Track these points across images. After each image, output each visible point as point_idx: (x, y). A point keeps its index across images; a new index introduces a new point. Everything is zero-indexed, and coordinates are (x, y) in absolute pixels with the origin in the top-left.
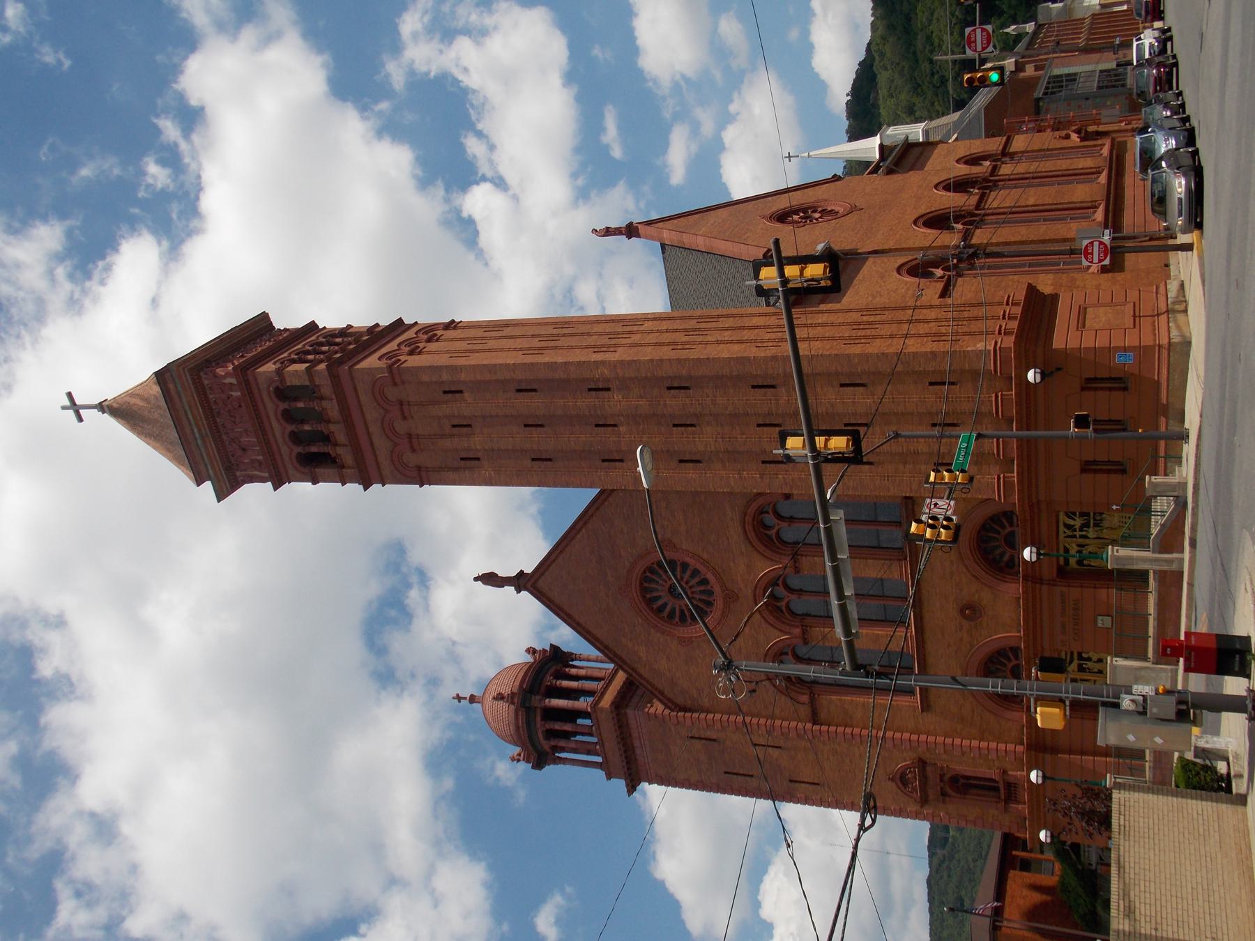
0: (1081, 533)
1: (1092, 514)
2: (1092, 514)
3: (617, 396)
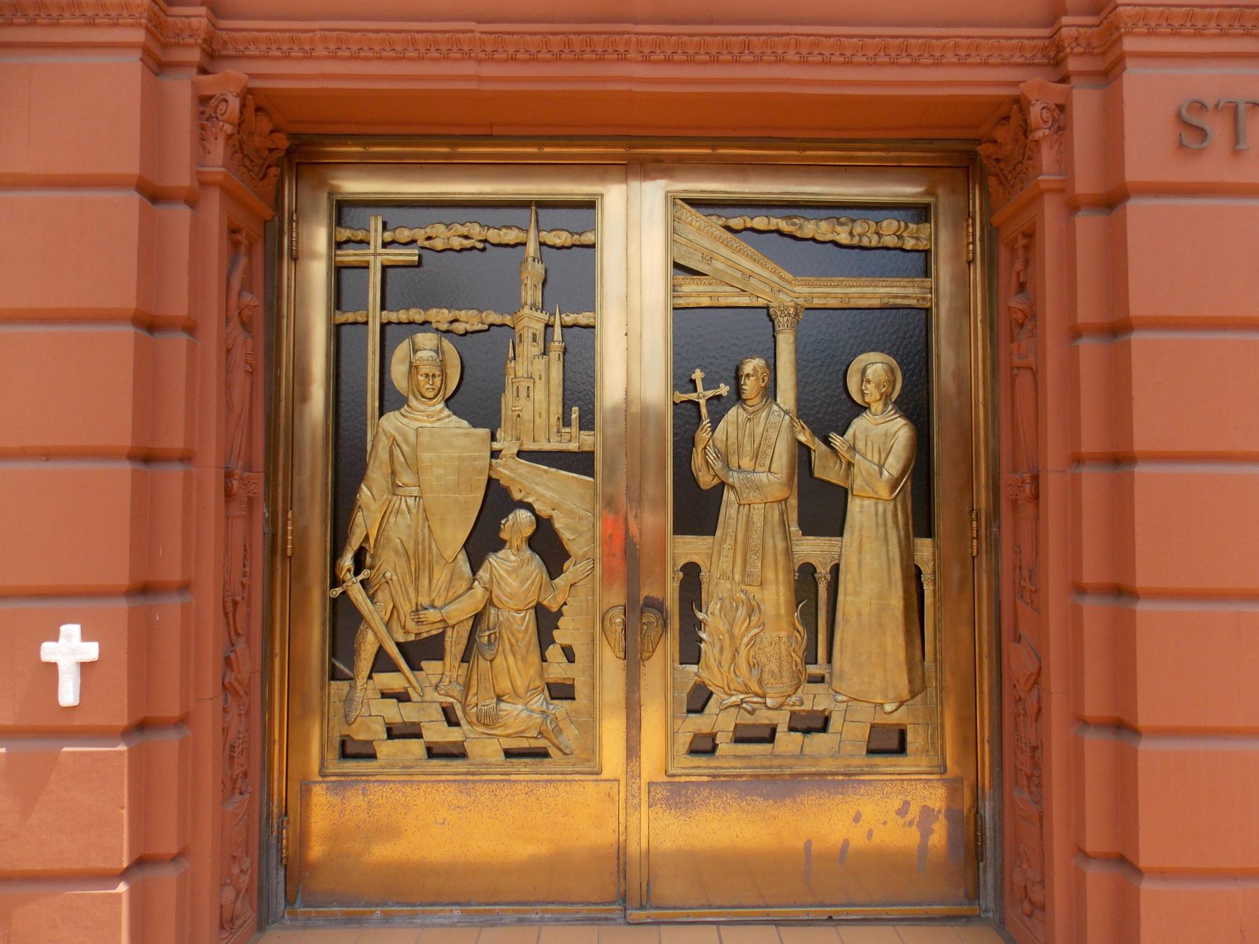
3: (1026, 795)
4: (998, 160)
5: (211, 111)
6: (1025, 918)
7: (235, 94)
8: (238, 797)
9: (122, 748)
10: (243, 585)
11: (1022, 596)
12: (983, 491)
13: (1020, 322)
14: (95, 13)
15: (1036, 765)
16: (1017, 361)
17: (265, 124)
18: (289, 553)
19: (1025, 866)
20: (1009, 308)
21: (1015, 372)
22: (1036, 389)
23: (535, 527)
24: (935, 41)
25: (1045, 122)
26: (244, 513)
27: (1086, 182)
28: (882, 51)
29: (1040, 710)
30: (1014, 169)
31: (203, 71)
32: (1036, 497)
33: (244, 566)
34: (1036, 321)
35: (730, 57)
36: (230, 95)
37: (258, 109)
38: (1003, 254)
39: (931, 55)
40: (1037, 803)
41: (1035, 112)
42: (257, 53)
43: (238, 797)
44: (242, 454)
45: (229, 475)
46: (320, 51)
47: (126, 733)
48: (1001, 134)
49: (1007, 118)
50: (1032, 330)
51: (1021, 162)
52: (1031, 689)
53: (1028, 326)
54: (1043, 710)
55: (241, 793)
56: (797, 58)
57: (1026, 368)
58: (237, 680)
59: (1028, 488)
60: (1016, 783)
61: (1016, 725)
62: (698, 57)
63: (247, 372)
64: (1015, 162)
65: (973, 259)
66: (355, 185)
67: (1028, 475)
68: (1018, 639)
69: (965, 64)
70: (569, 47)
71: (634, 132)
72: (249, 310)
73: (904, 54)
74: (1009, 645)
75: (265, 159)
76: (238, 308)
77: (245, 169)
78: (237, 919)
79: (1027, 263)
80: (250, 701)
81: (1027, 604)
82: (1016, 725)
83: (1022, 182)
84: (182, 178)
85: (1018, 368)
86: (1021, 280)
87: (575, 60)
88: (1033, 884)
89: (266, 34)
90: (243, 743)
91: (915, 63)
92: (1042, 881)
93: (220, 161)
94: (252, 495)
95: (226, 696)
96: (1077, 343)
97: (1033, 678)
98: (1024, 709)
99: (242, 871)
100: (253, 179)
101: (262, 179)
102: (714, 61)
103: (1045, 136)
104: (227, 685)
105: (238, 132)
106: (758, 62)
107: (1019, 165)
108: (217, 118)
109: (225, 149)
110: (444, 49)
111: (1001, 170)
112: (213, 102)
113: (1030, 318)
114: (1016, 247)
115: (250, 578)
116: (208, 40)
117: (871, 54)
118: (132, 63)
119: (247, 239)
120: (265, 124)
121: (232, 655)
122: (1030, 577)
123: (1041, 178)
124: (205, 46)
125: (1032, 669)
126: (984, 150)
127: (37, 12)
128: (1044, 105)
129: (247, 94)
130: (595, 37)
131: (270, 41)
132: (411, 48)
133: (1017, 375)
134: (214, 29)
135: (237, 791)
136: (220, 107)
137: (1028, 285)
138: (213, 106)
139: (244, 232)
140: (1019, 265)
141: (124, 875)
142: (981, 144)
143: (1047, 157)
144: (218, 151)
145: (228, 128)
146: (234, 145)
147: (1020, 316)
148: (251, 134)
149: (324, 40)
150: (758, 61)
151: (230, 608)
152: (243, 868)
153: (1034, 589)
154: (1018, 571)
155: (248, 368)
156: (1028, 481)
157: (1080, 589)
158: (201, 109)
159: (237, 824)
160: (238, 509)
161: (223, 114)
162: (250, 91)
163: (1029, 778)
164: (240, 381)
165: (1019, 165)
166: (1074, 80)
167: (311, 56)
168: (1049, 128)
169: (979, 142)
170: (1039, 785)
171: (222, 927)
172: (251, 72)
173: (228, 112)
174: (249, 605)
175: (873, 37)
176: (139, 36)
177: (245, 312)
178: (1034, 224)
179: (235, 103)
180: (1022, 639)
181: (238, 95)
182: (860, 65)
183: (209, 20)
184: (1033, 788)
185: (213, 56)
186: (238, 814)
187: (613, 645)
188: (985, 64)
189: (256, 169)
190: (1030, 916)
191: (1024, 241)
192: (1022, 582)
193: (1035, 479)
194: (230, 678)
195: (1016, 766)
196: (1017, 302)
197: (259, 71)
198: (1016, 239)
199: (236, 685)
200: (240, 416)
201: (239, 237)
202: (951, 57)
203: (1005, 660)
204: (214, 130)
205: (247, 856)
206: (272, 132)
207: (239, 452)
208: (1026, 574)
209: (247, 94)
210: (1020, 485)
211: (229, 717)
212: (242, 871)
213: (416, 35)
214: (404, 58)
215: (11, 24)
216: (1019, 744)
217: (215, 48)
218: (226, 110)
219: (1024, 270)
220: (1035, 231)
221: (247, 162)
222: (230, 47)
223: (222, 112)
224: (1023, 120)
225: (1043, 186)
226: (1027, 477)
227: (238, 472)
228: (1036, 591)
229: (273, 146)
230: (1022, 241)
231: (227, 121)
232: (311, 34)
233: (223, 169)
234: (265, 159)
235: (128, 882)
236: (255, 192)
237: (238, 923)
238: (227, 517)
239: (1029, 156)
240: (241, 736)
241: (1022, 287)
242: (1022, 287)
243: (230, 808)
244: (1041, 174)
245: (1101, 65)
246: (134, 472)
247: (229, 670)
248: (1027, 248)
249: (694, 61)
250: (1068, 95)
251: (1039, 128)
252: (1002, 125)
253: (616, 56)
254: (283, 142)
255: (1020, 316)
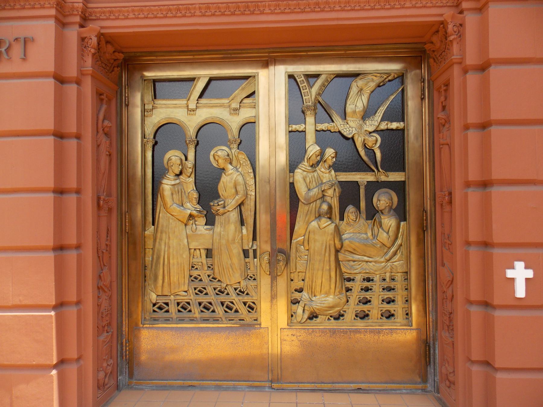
0: (311, 137)
1: (395, 177)
2: (395, 177)
3: (447, 334)
4: (434, 51)
5: (86, 43)
6: (447, 388)
7: (94, 36)
8: (105, 334)
9: (53, 313)
10: (107, 245)
11: (445, 246)
12: (428, 201)
13: (443, 124)
14: (34, 3)
15: (450, 320)
16: (442, 141)
17: (110, 49)
18: (127, 231)
19: (447, 365)
20: (438, 118)
21: (441, 146)
22: (451, 154)
23: (206, 220)
24: (270, 2)
25: (455, 32)
26: (106, 214)
27: (471, 59)
28: (377, 3)
29: (453, 296)
30: (441, 54)
31: (82, 26)
32: (450, 202)
33: (107, 237)
34: (450, 123)
35: (240, 13)
36: (93, 36)
37: (107, 42)
38: (436, 94)
39: (123, 15)
40: (452, 337)
41: (450, 27)
42: (105, 17)
43: (105, 334)
44: (105, 190)
45: (99, 198)
46: (267, 11)
47: (55, 308)
48: (435, 39)
49: (437, 31)
50: (449, 127)
51: (444, 51)
52: (449, 287)
53: (447, 126)
54: (454, 297)
55: (107, 332)
56: (270, 11)
57: (447, 144)
58: (103, 284)
59: (447, 198)
60: (443, 329)
61: (443, 303)
62: (295, 10)
63: (107, 155)
64: (441, 52)
65: (424, 98)
66: (149, 74)
67: (447, 192)
68: (443, 265)
69: (294, 12)
70: (238, 9)
71: (211, 48)
72: (107, 128)
73: (317, 7)
74: (440, 268)
75: (112, 64)
76: (103, 127)
77: (103, 68)
78: (106, 385)
79: (446, 98)
80: (112, 293)
81: (447, 250)
82: (443, 303)
83: (445, 60)
84: (72, 72)
85: (442, 145)
86: (443, 105)
87: (202, 16)
88: (450, 373)
89: (108, 9)
90: (107, 311)
91: (392, 8)
92: (454, 372)
93: (90, 65)
94: (110, 207)
95: (99, 292)
96: (467, 132)
97: (450, 282)
98: (446, 296)
99: (108, 365)
100: (107, 72)
101: (111, 73)
102: (303, 12)
103: (454, 39)
104: (99, 287)
105: (98, 52)
106: (343, 10)
107: (443, 52)
108: (88, 47)
109: (92, 60)
110: (242, 10)
111: (435, 55)
112: (86, 40)
113: (448, 121)
114: (441, 91)
115: (110, 241)
116: (84, 12)
117: (164, 13)
118: (52, 23)
119: (106, 97)
120: (110, 49)
121: (102, 275)
122: (448, 237)
123: (453, 57)
124: (82, 15)
125: (450, 279)
126: (427, 47)
127: (25, 3)
128: (453, 25)
129: (100, 36)
130: (230, 4)
131: (111, 12)
132: (169, 13)
133: (442, 148)
134: (86, 8)
135: (106, 331)
136: (89, 42)
137: (446, 107)
138: (86, 41)
139: (105, 95)
140: (442, 98)
141: (55, 367)
142: (426, 44)
143: (455, 48)
144: (89, 61)
145: (93, 51)
146: (97, 58)
147: (443, 121)
148: (104, 53)
149: (133, 11)
150: (252, 13)
151: (99, 254)
152: (108, 364)
153: (450, 243)
154: (443, 235)
155: (108, 153)
156: (447, 195)
157: (468, 243)
158: (82, 43)
159: (105, 345)
160: (103, 213)
161: (90, 45)
162: (102, 34)
163: (448, 327)
164: (104, 160)
165: (443, 52)
166: (465, 13)
167: (304, 11)
168: (457, 35)
169: (425, 43)
170: (452, 330)
171: (99, 388)
172: (102, 25)
173: (93, 43)
174: (110, 253)
175: (164, 6)
176: (53, 12)
177: (106, 129)
178: (449, 80)
179: (95, 40)
180: (445, 265)
181: (96, 36)
182: (160, 18)
183: (83, 4)
184: (450, 331)
185: (85, 19)
186: (106, 341)
187: (264, 269)
188: (425, 7)
189: (108, 68)
190: (449, 387)
191: (445, 88)
192: (445, 240)
193: (450, 194)
194: (101, 284)
195: (443, 321)
196: (441, 115)
197: (104, 25)
198: (440, 87)
199: (104, 287)
200: (104, 174)
201: (102, 97)
202: (337, 8)
203: (438, 273)
204: (86, 51)
205: (111, 358)
206: (114, 52)
207: (104, 190)
208: (447, 237)
209: (100, 36)
210: (444, 197)
211: (101, 300)
212: (108, 365)
213: (143, 8)
214: (384, 8)
215: (4, 9)
216: (444, 312)
217: (87, 16)
218: (91, 43)
219: (445, 101)
220: (449, 83)
221: (104, 66)
222: (93, 15)
223: (90, 44)
224: (445, 32)
225: (455, 61)
226: (447, 193)
227: (102, 197)
228: (451, 244)
229: (116, 58)
230: (444, 88)
231: (92, 48)
232: (127, 8)
233: (91, 69)
234: (112, 64)
235: (57, 370)
236: (108, 78)
237: (106, 387)
238: (99, 216)
239: (448, 48)
240: (106, 308)
241: (444, 108)
242: (444, 108)
243: (102, 338)
244: (453, 55)
245: (478, 5)
246: (55, 197)
247: (100, 281)
248: (446, 91)
249: (384, 9)
250: (464, 19)
251: (452, 35)
252: (436, 35)
253: (329, 9)
254: (121, 56)
255: (443, 121)
